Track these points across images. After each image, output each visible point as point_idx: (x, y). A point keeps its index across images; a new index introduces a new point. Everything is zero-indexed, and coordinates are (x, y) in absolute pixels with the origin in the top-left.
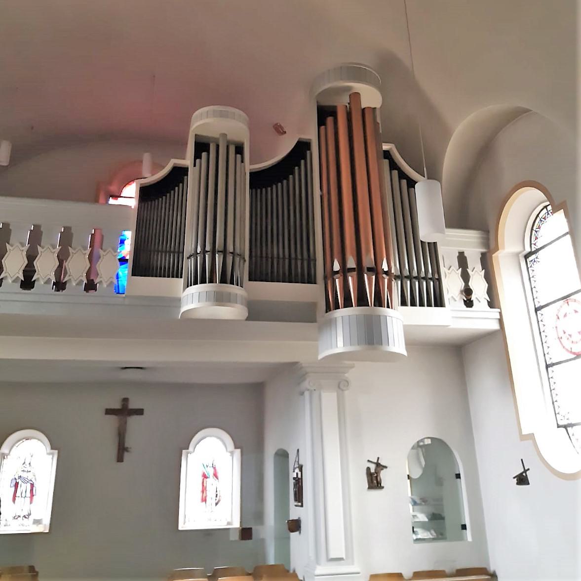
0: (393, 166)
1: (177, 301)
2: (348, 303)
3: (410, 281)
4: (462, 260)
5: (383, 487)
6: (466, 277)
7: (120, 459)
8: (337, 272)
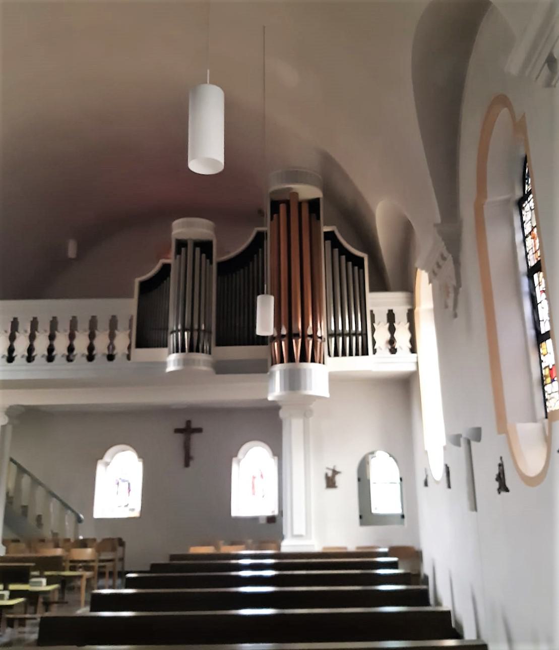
0: (336, 244)
1: (164, 364)
2: (282, 361)
3: (350, 337)
4: (391, 317)
5: (499, 493)
6: (392, 330)
7: (187, 464)
8: (283, 336)
